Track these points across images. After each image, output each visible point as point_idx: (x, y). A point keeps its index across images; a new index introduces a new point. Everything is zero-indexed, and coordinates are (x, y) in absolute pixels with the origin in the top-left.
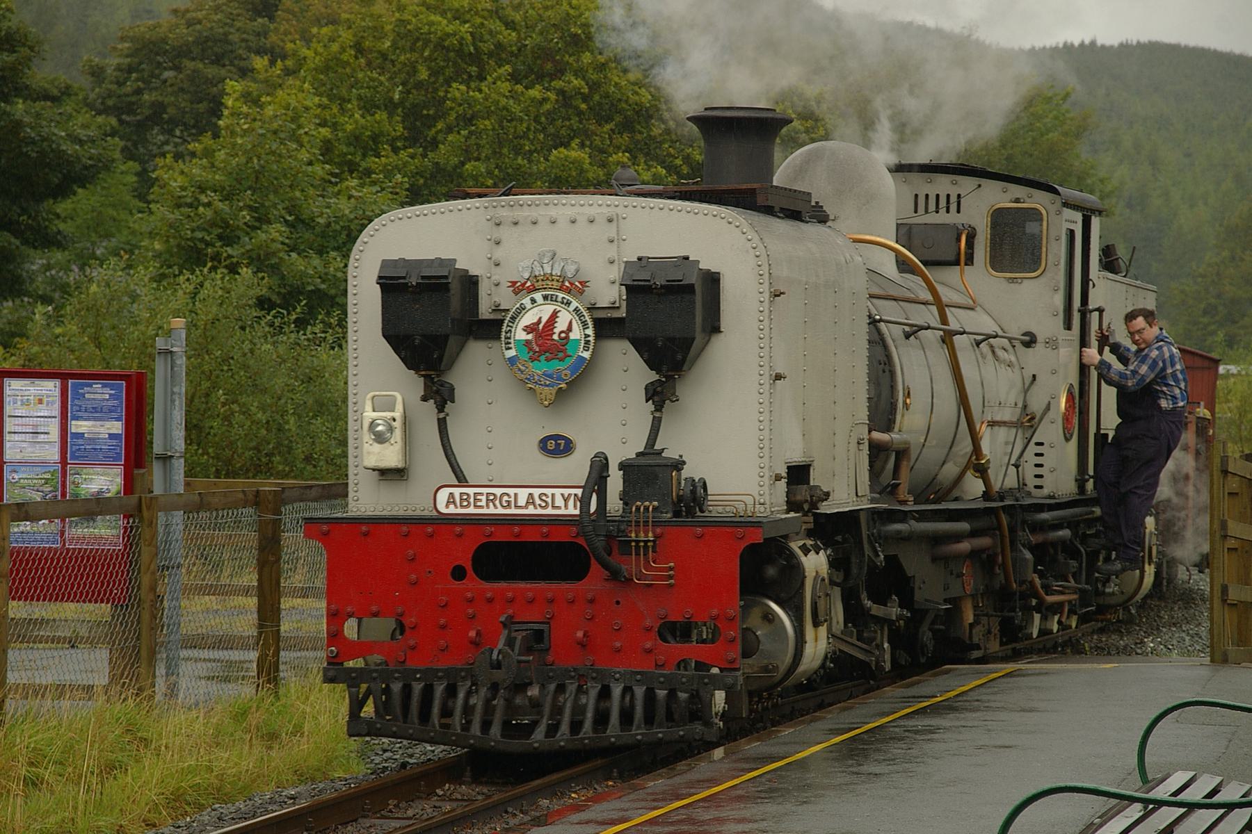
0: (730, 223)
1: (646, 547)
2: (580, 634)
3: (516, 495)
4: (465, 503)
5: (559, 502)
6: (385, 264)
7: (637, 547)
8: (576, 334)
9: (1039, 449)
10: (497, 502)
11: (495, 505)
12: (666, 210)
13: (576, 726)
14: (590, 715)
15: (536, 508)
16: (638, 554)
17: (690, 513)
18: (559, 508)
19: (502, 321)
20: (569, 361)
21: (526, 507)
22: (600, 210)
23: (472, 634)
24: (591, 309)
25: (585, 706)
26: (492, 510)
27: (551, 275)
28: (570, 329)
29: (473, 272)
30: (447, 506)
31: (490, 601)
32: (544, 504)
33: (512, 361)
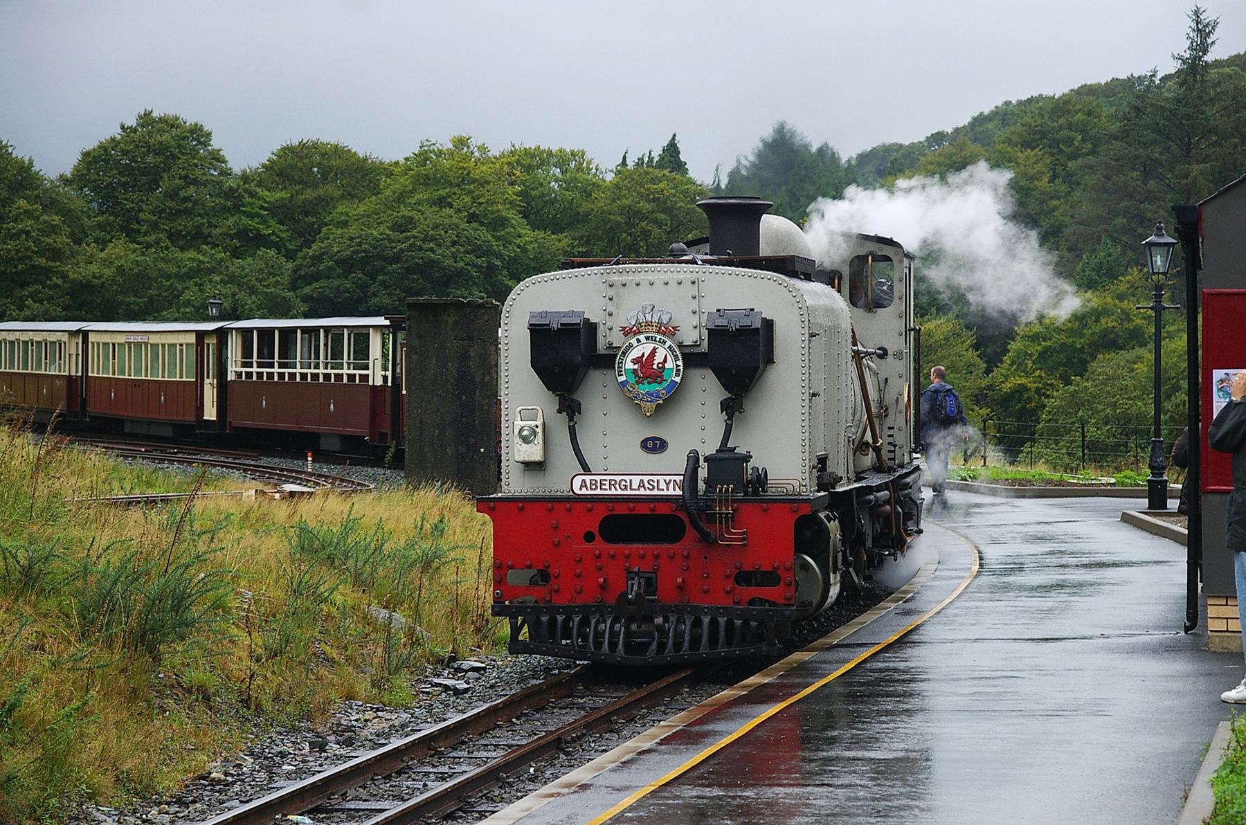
0: (780, 284)
1: (727, 517)
2: (679, 580)
3: (631, 480)
4: (594, 487)
5: (662, 485)
6: (532, 316)
7: (721, 518)
8: (669, 365)
9: (891, 432)
10: (617, 486)
11: (616, 489)
12: (734, 275)
13: (678, 646)
14: (687, 638)
15: (645, 490)
16: (721, 523)
17: (756, 493)
18: (663, 490)
19: (616, 355)
20: (665, 384)
21: (639, 489)
22: (671, 275)
23: (601, 580)
24: (680, 346)
25: (684, 633)
26: (613, 492)
27: (652, 322)
28: (665, 360)
29: (593, 320)
30: (581, 489)
31: (613, 557)
32: (651, 487)
33: (623, 384)
